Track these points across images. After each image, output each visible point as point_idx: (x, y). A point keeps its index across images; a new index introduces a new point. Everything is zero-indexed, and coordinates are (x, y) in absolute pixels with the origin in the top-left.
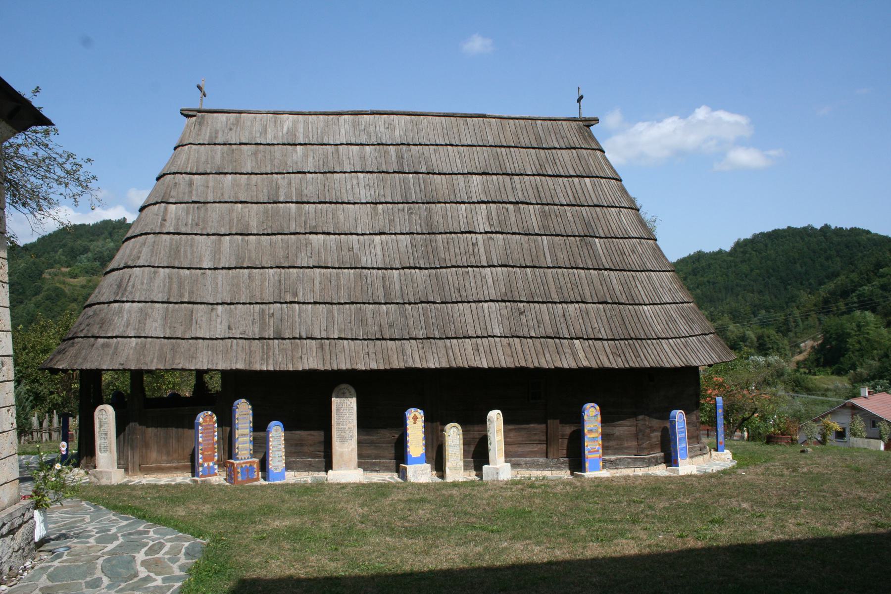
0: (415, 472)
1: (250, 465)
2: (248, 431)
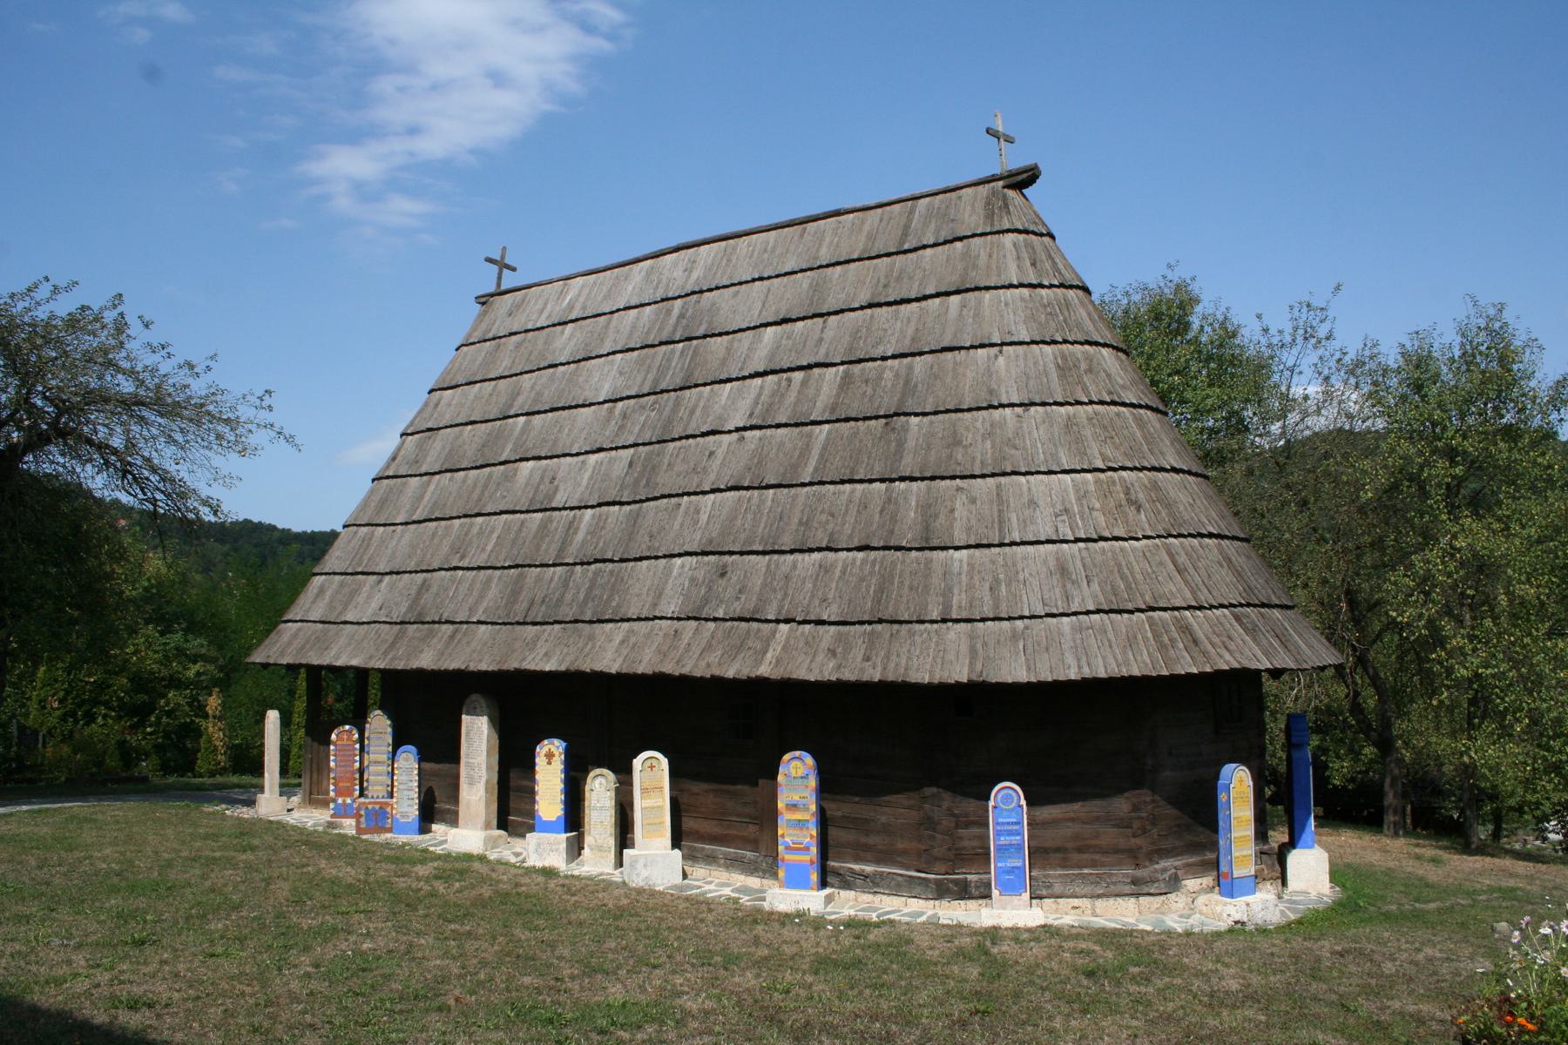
0: (539, 844)
1: (381, 808)
2: (385, 756)
